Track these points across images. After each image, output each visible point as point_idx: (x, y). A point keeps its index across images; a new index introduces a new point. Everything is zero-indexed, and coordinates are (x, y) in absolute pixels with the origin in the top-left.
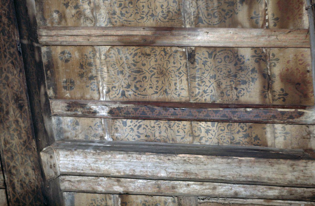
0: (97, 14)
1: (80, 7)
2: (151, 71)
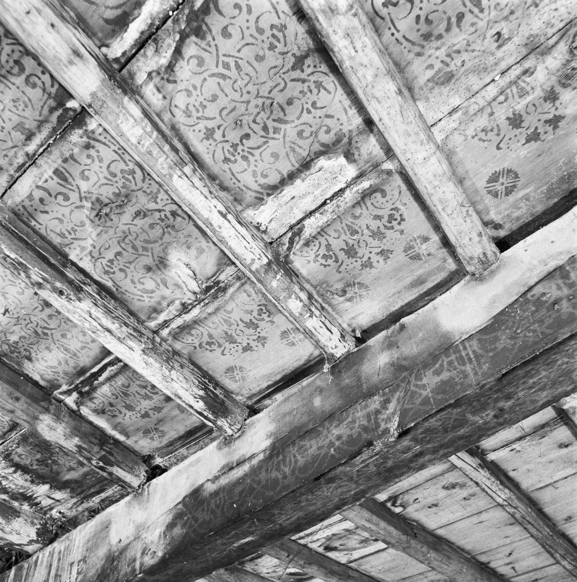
0: (551, 32)
1: (549, 89)
2: (226, 66)
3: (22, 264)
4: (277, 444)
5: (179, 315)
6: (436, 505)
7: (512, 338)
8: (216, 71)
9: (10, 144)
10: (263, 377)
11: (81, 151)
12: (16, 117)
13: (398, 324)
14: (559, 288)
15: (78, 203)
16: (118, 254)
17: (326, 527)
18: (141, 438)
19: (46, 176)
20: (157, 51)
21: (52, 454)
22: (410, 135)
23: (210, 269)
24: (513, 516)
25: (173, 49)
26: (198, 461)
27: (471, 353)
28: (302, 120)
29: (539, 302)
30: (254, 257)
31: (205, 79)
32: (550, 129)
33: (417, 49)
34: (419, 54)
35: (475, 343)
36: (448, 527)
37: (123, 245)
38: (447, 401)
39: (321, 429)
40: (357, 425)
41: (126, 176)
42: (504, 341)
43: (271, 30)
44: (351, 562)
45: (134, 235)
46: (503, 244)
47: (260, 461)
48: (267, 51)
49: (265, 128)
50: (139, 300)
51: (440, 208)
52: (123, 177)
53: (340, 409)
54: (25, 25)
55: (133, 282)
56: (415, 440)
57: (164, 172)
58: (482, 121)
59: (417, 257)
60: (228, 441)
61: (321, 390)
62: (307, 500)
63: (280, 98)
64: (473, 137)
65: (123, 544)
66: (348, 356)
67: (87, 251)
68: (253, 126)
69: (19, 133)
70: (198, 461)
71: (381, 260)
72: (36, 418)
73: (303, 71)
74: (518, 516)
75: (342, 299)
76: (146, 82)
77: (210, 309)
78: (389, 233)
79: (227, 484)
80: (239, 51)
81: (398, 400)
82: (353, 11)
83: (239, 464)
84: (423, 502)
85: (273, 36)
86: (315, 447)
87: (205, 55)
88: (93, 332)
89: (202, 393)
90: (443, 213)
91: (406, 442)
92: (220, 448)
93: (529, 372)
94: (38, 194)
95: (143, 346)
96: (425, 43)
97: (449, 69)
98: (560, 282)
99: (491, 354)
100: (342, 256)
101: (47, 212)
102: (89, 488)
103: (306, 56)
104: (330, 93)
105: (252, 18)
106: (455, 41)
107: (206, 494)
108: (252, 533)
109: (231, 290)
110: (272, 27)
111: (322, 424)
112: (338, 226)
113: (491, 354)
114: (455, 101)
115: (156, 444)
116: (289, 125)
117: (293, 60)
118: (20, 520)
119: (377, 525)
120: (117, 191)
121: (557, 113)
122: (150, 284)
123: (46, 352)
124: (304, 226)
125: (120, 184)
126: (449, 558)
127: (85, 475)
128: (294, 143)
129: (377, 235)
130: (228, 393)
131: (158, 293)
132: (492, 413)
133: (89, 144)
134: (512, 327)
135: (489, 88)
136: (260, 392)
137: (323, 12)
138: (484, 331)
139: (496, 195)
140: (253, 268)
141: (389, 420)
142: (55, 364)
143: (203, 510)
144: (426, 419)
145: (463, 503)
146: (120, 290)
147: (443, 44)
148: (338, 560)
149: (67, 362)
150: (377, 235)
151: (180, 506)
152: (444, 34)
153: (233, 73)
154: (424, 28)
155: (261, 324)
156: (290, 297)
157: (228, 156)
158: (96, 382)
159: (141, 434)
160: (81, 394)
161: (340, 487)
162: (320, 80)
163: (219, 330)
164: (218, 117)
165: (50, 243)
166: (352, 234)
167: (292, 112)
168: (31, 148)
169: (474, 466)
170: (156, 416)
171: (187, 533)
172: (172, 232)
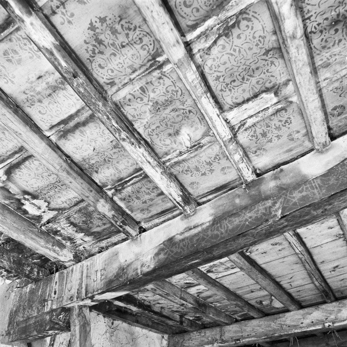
2: (235, 50)
3: (119, 129)
4: (216, 219)
5: (177, 157)
6: (265, 253)
7: (336, 180)
8: (229, 52)
9: (124, 74)
11: (156, 80)
12: (131, 62)
13: (279, 169)
15: (147, 103)
16: (158, 127)
18: (138, 213)
19: (136, 89)
20: (206, 41)
21: (91, 218)
22: (310, 90)
23: (198, 137)
24: (301, 259)
25: (213, 41)
26: (170, 225)
27: (317, 185)
28: (260, 77)
30: (226, 135)
31: (223, 55)
35: (319, 181)
36: (268, 264)
37: (161, 123)
38: (305, 204)
39: (240, 213)
40: (260, 212)
41: (174, 93)
42: (332, 181)
43: (259, 38)
44: (217, 279)
45: (168, 119)
46: (333, 138)
47: (207, 226)
48: (254, 46)
49: (243, 79)
50: (160, 148)
51: (313, 121)
52: (172, 93)
53: (250, 205)
54: (160, 28)
55: (160, 140)
57: (199, 95)
58: (336, 84)
59: (292, 139)
62: (231, 244)
64: (331, 91)
66: (253, 181)
67: (144, 124)
69: (130, 69)
70: (170, 225)
72: (98, 201)
73: (267, 56)
74: (303, 259)
75: (254, 155)
77: (192, 155)
78: (283, 128)
79: (190, 236)
80: (242, 45)
81: (281, 202)
82: (302, 38)
84: (260, 251)
85: (259, 40)
86: (238, 221)
87: (226, 45)
88: (141, 163)
89: (181, 193)
90: (314, 123)
91: (282, 221)
92: (182, 219)
93: (342, 194)
95: (162, 170)
96: (322, 50)
97: (329, 62)
99: (327, 186)
100: (260, 136)
101: (130, 105)
102: (103, 236)
104: (276, 66)
105: (253, 32)
106: (335, 50)
107: (176, 240)
108: (199, 258)
109: (204, 148)
110: (260, 36)
111: (241, 211)
112: (262, 123)
113: (327, 186)
115: (145, 216)
116: (254, 78)
117: (265, 51)
118: (66, 249)
119: (241, 260)
120: (167, 99)
122: (168, 142)
124: (247, 122)
125: (169, 96)
126: (266, 277)
127: (104, 230)
128: (254, 86)
130: (189, 194)
131: (171, 146)
132: (322, 211)
133: (161, 77)
134: (337, 175)
135: (343, 71)
136: (203, 195)
137: (290, 37)
138: (324, 175)
140: (224, 140)
141: (276, 211)
142: (109, 175)
143: (176, 247)
145: (278, 252)
146: (153, 143)
147: (330, 51)
148: (212, 277)
149: (115, 175)
150: (278, 128)
151: (162, 245)
152: (331, 47)
153: (237, 54)
156: (236, 153)
157: (223, 88)
158: (126, 185)
159: (139, 211)
160: (116, 190)
161: (247, 239)
162: (273, 60)
163: (193, 165)
164: (224, 71)
165: (127, 119)
166: (267, 127)
167: (257, 73)
168: (132, 77)
169: (291, 234)
171: (167, 258)
172: (186, 119)
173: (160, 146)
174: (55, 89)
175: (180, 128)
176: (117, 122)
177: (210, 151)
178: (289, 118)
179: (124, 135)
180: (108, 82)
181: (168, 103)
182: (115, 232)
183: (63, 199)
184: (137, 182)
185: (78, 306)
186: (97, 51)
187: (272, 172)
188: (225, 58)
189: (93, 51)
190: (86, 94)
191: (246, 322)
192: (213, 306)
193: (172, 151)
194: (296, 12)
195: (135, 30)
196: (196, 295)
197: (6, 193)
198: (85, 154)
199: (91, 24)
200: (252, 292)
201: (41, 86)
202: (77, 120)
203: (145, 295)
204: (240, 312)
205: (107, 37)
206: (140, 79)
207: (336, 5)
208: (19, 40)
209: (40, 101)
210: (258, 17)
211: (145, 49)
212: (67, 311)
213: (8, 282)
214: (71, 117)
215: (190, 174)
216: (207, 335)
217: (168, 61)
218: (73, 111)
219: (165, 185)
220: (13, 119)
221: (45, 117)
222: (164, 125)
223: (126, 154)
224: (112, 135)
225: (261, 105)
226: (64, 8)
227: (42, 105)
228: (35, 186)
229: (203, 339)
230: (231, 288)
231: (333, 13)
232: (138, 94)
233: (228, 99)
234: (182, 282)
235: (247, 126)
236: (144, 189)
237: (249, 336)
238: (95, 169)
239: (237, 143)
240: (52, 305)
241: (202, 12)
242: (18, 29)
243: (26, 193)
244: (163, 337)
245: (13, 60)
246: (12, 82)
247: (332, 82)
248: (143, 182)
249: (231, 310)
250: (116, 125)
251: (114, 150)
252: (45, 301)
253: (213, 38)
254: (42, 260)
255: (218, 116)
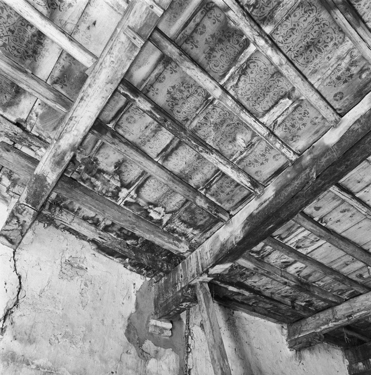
0: (343, 54)
2: (252, 81)
6: (339, 221)
10: (268, 173)
14: (358, 125)
16: (221, 139)
17: (296, 236)
23: (249, 139)
26: (249, 206)
28: (275, 90)
29: (353, 131)
32: (350, 78)
33: (305, 66)
34: (306, 67)
35: (336, 146)
36: (346, 231)
42: (344, 144)
46: (341, 116)
49: (264, 95)
51: (319, 108)
55: (225, 147)
56: (321, 179)
58: (328, 80)
59: (315, 124)
60: (259, 197)
61: (289, 172)
62: (290, 206)
63: (268, 86)
65: (226, 240)
66: (297, 160)
68: (261, 95)
71: (303, 127)
76: (230, 89)
77: (249, 152)
78: (304, 118)
83: (265, 202)
84: (333, 220)
89: (249, 180)
91: (319, 180)
92: (256, 200)
94: (198, 125)
98: (358, 124)
100: (291, 128)
103: (274, 74)
107: (254, 214)
109: (256, 145)
110: (264, 69)
111: (292, 182)
112: (288, 119)
114: (319, 77)
115: (231, 205)
119: (316, 228)
121: (352, 73)
122: (230, 147)
123: (197, 175)
125: (222, 118)
129: (301, 119)
131: (233, 149)
135: (328, 71)
139: (337, 100)
141: (313, 174)
144: (324, 171)
145: (350, 218)
150: (301, 119)
153: (254, 82)
154: (306, 60)
155: (266, 154)
160: (206, 189)
167: (271, 89)
170: (232, 194)
173: (227, 152)
174: (156, 131)
175: (235, 136)
176: (195, 142)
177: (260, 146)
178: (306, 110)
179: (200, 148)
180: (184, 119)
181: (223, 122)
182: (214, 222)
183: (174, 203)
184: (219, 180)
185: (199, 282)
186: (174, 104)
187: (308, 150)
188: (248, 86)
189: (172, 105)
190: (174, 129)
191: (355, 299)
192: (317, 286)
193: (235, 153)
194: (277, 52)
195: (192, 87)
196: (296, 275)
197: (138, 207)
198: (181, 168)
199: (168, 91)
200: (347, 265)
201: (148, 132)
202: (171, 147)
203: (253, 280)
204: (347, 290)
205: (178, 95)
206: (202, 112)
207: (303, 38)
208: (133, 110)
209: (149, 141)
210: (259, 59)
211: (200, 95)
212: (193, 287)
213: (148, 279)
214: (168, 146)
215: (253, 166)
216: (321, 317)
217: (214, 99)
218: (168, 142)
219: (236, 176)
220: (136, 155)
221: (153, 149)
222: (225, 137)
223: (206, 162)
224: (194, 151)
225: (283, 107)
226: (153, 87)
227: (150, 143)
228: (155, 197)
229: (318, 322)
230: (325, 262)
231: (303, 43)
232: (203, 121)
233: (259, 109)
234: (280, 261)
235: (278, 123)
236: (224, 184)
237: (359, 311)
238: (189, 177)
239: (275, 136)
240: (181, 285)
241: (226, 67)
242: (132, 105)
243: (149, 203)
244: (283, 327)
245: (131, 122)
246: (133, 134)
247: (324, 80)
248: (223, 179)
249: (337, 289)
250: (195, 144)
251: (198, 161)
252: (176, 284)
253: (237, 78)
254: (168, 256)
255: (255, 122)
